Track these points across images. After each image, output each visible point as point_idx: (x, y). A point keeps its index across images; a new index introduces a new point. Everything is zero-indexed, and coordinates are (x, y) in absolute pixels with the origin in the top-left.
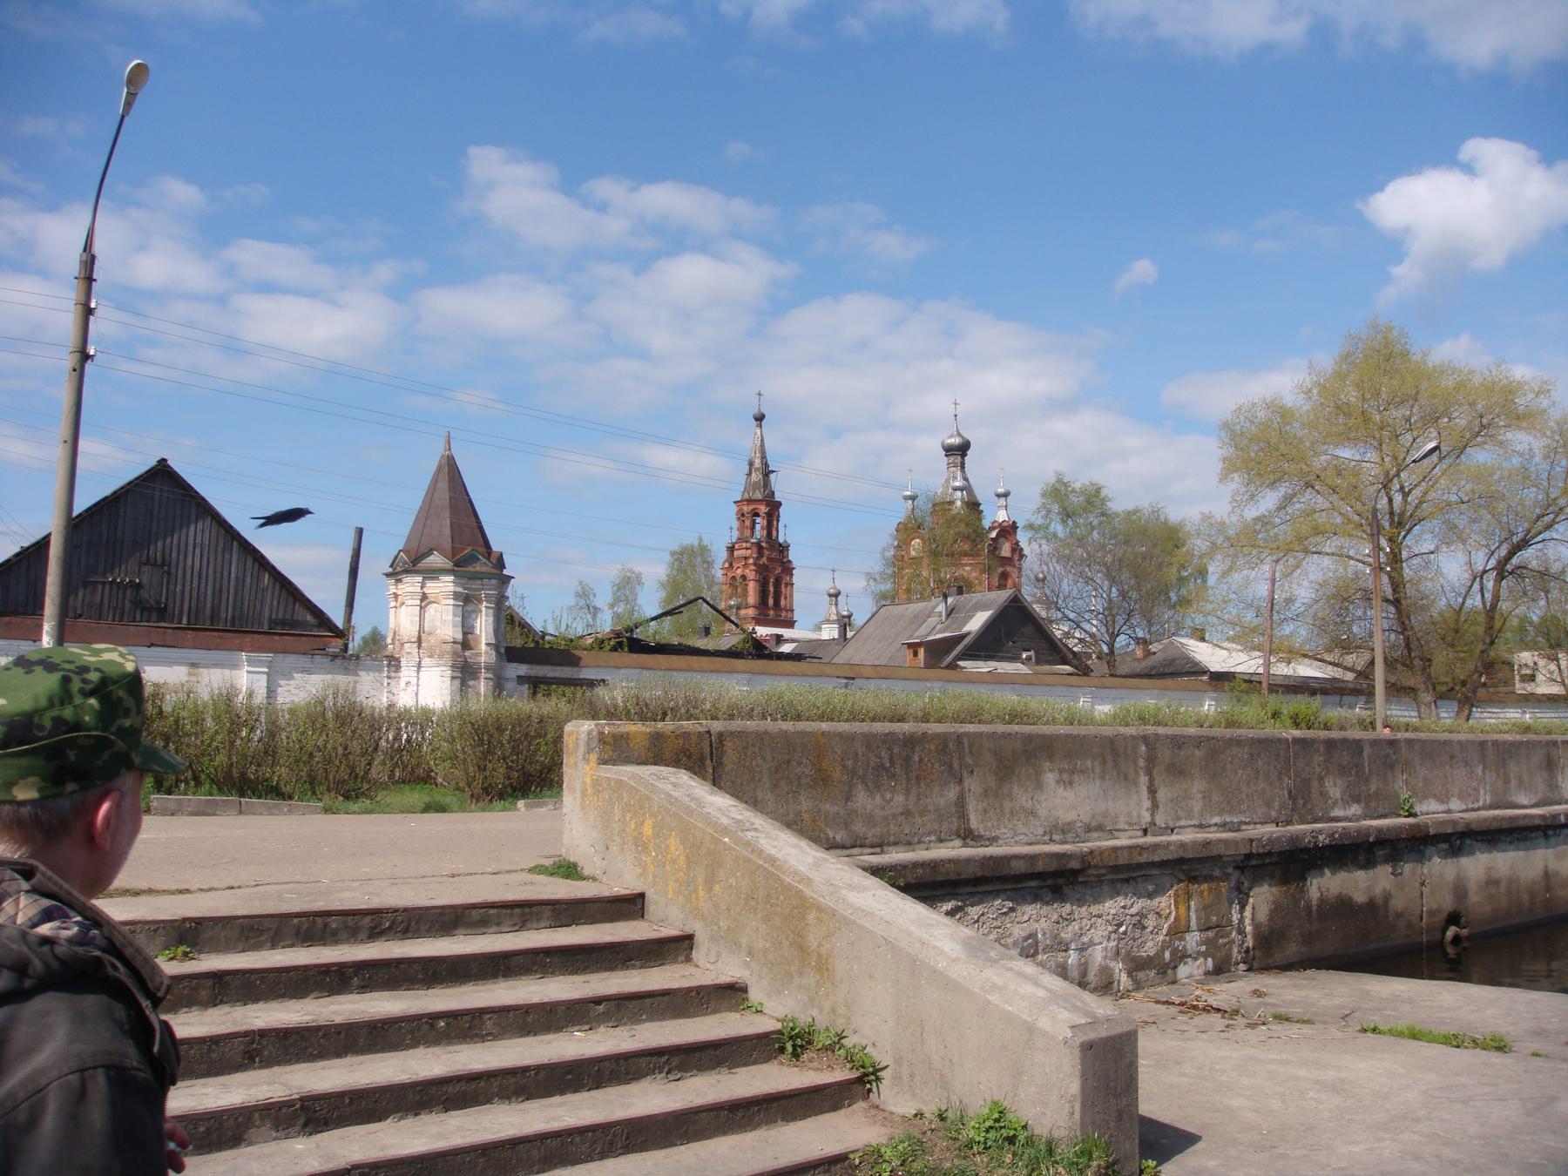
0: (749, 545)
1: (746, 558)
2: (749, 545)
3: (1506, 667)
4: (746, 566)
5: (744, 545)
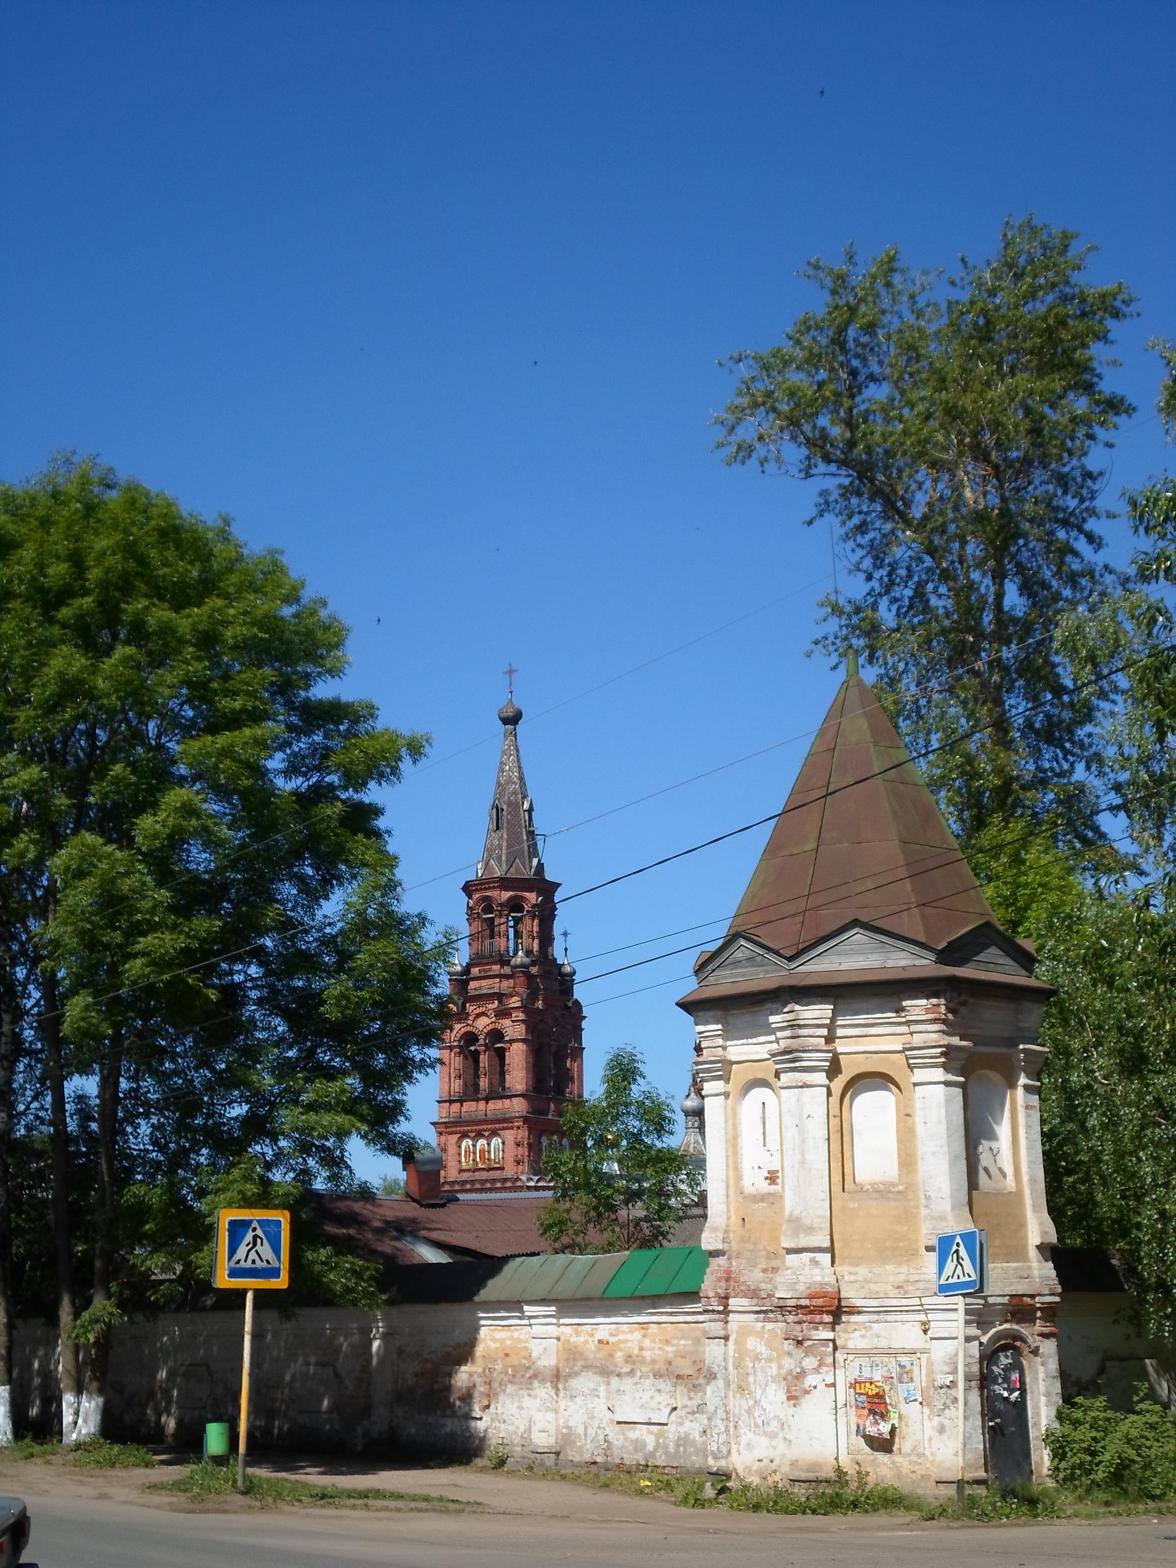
0: (507, 970)
1: (499, 996)
2: (507, 970)
4: (503, 1013)
5: (496, 968)
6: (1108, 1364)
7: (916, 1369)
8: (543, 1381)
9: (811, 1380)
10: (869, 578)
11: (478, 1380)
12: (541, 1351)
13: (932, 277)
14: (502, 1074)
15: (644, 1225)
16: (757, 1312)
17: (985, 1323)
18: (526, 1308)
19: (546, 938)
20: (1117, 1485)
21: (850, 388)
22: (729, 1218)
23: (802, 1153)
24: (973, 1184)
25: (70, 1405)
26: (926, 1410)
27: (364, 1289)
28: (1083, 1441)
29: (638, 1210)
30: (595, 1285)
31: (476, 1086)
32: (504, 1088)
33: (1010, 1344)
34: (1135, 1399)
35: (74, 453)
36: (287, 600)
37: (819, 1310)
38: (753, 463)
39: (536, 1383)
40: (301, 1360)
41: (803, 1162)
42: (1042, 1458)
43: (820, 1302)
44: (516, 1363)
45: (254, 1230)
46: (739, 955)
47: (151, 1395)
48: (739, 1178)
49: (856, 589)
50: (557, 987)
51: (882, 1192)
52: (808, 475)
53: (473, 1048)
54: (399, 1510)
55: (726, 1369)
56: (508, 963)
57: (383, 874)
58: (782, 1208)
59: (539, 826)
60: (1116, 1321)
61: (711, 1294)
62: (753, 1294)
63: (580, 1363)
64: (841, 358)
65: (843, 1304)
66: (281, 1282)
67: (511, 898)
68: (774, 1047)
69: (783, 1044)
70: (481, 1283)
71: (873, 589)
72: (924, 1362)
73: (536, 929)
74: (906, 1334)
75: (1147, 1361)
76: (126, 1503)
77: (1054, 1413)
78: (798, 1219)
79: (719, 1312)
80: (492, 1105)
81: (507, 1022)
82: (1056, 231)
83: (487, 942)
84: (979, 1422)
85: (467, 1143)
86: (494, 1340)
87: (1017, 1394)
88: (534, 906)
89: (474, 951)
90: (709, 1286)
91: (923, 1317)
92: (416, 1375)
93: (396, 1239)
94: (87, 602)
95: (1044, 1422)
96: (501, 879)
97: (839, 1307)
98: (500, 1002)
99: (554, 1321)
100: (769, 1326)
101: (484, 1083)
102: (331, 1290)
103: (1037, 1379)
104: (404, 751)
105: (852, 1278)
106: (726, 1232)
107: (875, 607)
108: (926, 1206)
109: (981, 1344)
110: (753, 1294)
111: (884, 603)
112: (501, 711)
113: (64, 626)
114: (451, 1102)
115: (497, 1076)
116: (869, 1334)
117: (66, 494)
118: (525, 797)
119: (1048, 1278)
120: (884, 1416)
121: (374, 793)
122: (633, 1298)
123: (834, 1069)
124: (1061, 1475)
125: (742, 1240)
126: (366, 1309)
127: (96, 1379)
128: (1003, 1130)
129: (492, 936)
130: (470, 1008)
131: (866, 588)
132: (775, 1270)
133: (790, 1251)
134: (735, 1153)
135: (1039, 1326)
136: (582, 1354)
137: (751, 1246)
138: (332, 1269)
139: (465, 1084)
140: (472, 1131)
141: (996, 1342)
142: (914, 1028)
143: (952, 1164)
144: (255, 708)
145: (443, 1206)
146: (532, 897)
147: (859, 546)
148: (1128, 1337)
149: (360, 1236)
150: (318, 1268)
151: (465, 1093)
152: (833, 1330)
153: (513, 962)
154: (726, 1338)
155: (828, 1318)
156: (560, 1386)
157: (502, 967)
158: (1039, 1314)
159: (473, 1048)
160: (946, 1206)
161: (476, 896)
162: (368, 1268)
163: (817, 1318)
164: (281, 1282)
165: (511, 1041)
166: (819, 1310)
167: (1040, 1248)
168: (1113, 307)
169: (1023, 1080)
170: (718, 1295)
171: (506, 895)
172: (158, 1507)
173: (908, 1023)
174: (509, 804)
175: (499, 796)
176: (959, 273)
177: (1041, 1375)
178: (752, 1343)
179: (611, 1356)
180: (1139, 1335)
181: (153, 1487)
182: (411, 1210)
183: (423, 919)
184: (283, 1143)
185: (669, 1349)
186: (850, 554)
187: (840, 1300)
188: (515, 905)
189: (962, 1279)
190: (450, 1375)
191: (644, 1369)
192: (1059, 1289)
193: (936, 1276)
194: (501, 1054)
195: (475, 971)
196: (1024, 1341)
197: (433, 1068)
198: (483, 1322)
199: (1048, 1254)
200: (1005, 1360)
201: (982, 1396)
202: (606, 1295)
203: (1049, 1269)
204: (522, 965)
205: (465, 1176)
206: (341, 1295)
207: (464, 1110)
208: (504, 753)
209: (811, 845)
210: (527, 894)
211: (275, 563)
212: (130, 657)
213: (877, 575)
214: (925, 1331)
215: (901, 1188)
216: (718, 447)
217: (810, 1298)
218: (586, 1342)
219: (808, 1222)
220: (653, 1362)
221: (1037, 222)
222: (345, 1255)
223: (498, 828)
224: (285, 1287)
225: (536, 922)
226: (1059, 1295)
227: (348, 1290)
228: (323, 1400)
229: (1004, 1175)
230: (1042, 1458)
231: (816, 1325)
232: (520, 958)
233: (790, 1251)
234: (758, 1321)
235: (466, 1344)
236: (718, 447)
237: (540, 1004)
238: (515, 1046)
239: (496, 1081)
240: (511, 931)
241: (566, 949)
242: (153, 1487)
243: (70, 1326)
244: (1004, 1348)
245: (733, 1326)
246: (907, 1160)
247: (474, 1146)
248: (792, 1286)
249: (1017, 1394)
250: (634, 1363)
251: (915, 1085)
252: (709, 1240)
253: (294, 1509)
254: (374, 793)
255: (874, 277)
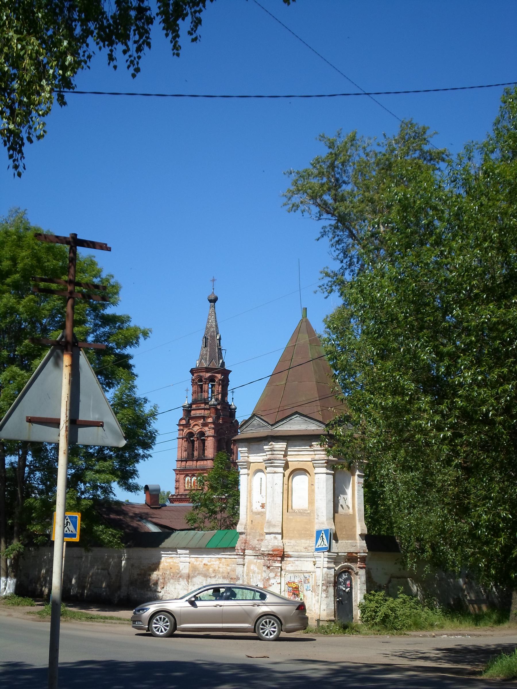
0: (207, 406)
1: (204, 418)
2: (207, 406)
3: (382, 580)
4: (205, 425)
5: (203, 406)
6: (392, 579)
7: (310, 578)
8: (183, 579)
9: (272, 581)
10: (342, 262)
11: (160, 578)
12: (183, 567)
13: (372, 141)
14: (204, 450)
15: (227, 520)
16: (255, 556)
17: (337, 562)
18: (178, 551)
19: (224, 394)
20: (383, 624)
21: (336, 186)
22: (247, 520)
23: (273, 498)
24: (335, 511)
25: (3, 582)
26: (313, 594)
27: (116, 542)
28: (372, 607)
29: (225, 515)
30: (203, 543)
31: (193, 454)
32: (204, 456)
33: (347, 571)
34: (398, 593)
35: (19, 209)
36: (95, 276)
37: (276, 556)
38: (299, 212)
39: (181, 579)
40: (96, 567)
41: (273, 501)
42: (357, 613)
43: (276, 553)
44: (174, 571)
45: (67, 519)
46: (254, 422)
47: (39, 578)
48: (251, 506)
49: (336, 266)
50: (228, 414)
51: (302, 513)
52: (320, 219)
53: (192, 439)
54: (115, 623)
55: (243, 576)
56: (208, 403)
57: (129, 384)
58: (265, 517)
59: (223, 346)
60: (396, 563)
61: (239, 548)
62: (254, 549)
63: (197, 572)
64: (333, 173)
65: (285, 553)
66: (77, 539)
67: (210, 376)
68: (265, 458)
69: (268, 457)
70: (163, 541)
71: (343, 266)
72: (313, 576)
73: (220, 390)
74: (307, 565)
75: (409, 579)
76: (17, 618)
77: (363, 597)
78: (270, 522)
79: (242, 555)
80: (199, 463)
81: (206, 429)
82: (421, 126)
83: (200, 394)
84: (333, 599)
85: (188, 478)
86: (167, 563)
87: (349, 589)
88: (220, 380)
89: (194, 398)
90: (239, 545)
91: (314, 560)
92: (138, 575)
93: (139, 521)
94: (17, 276)
95: (359, 600)
96: (206, 368)
97: (284, 555)
98: (204, 420)
99: (188, 556)
100: (259, 561)
101: (196, 453)
102: (103, 541)
103: (357, 584)
104: (141, 336)
105: (289, 544)
106: (245, 525)
107: (343, 274)
108: (317, 519)
109: (335, 570)
110: (254, 549)
111: (347, 272)
112: (209, 297)
113: (8, 285)
114: (182, 461)
115: (202, 451)
116: (294, 565)
117: (10, 232)
118: (218, 333)
119: (363, 547)
120: (298, 595)
121: (128, 351)
122: (216, 548)
123: (286, 466)
124: (364, 620)
125: (251, 529)
126: (117, 549)
127: (13, 572)
128: (349, 491)
129: (202, 392)
130: (191, 422)
131: (340, 265)
132: (262, 540)
133: (267, 534)
134: (250, 496)
135: (359, 564)
136: (198, 569)
137: (254, 531)
138: (104, 533)
139: (188, 454)
140: (190, 474)
141: (343, 569)
142: (316, 453)
143: (327, 504)
144: (80, 319)
145: (160, 508)
146: (219, 376)
147: (337, 249)
148: (400, 569)
149: (124, 519)
150: (99, 533)
151: (188, 458)
152: (281, 563)
153: (210, 403)
154: (244, 565)
155: (279, 559)
156: (190, 581)
157: (205, 405)
158: (359, 560)
159: (192, 439)
160: (324, 519)
161: (195, 375)
162: (118, 534)
163: (275, 558)
164: (77, 539)
165: (208, 437)
166: (276, 556)
167: (361, 535)
168: (442, 157)
169: (358, 473)
170: (241, 549)
171: (208, 375)
172: (28, 620)
173: (314, 451)
174: (211, 336)
175: (207, 333)
176: (382, 140)
177: (359, 582)
178: (252, 567)
179: (208, 570)
180: (404, 569)
181: (29, 613)
182: (148, 510)
183: (146, 400)
184: (88, 485)
185: (229, 568)
186: (333, 252)
187: (284, 552)
188: (212, 379)
189: (323, 546)
190: (150, 575)
191: (219, 575)
192: (367, 551)
193: (314, 545)
194: (203, 441)
195: (194, 406)
196: (353, 570)
197: (147, 458)
198: (163, 555)
199: (364, 538)
200: (344, 576)
201: (334, 589)
202: (207, 547)
203: (364, 543)
204: (214, 405)
205: (187, 492)
206: (107, 544)
207: (187, 464)
208: (209, 315)
209: (284, 382)
210: (217, 375)
211: (92, 261)
212: (32, 299)
213: (345, 261)
214: (314, 565)
215: (309, 512)
216: (284, 205)
217: (273, 551)
218: (199, 564)
219: (274, 523)
220: (223, 573)
221: (414, 122)
222: (109, 528)
223: (206, 346)
224: (78, 541)
225: (220, 386)
226: (367, 553)
227: (110, 542)
228: (76, 582)
229: (349, 508)
230: (357, 613)
231: (275, 561)
232: (213, 402)
233: (267, 534)
234: (255, 559)
235: (156, 564)
236: (284, 205)
237: (221, 421)
238: (210, 438)
239: (201, 453)
240: (210, 390)
241: (233, 398)
242: (29, 613)
243: (4, 550)
244: (344, 572)
245: (246, 560)
246: (311, 501)
247: (191, 480)
248: (267, 546)
249: (349, 589)
250: (216, 573)
251: (315, 474)
252: (239, 528)
253: (77, 622)
254: (128, 351)
255: (346, 143)
